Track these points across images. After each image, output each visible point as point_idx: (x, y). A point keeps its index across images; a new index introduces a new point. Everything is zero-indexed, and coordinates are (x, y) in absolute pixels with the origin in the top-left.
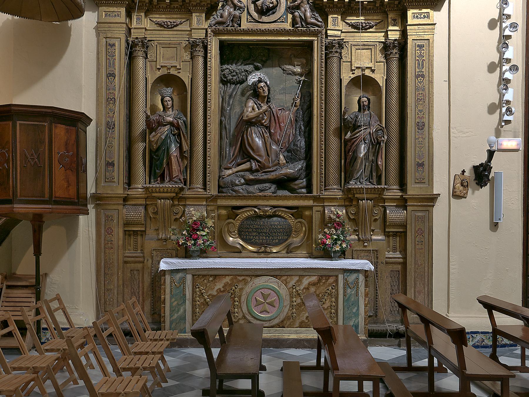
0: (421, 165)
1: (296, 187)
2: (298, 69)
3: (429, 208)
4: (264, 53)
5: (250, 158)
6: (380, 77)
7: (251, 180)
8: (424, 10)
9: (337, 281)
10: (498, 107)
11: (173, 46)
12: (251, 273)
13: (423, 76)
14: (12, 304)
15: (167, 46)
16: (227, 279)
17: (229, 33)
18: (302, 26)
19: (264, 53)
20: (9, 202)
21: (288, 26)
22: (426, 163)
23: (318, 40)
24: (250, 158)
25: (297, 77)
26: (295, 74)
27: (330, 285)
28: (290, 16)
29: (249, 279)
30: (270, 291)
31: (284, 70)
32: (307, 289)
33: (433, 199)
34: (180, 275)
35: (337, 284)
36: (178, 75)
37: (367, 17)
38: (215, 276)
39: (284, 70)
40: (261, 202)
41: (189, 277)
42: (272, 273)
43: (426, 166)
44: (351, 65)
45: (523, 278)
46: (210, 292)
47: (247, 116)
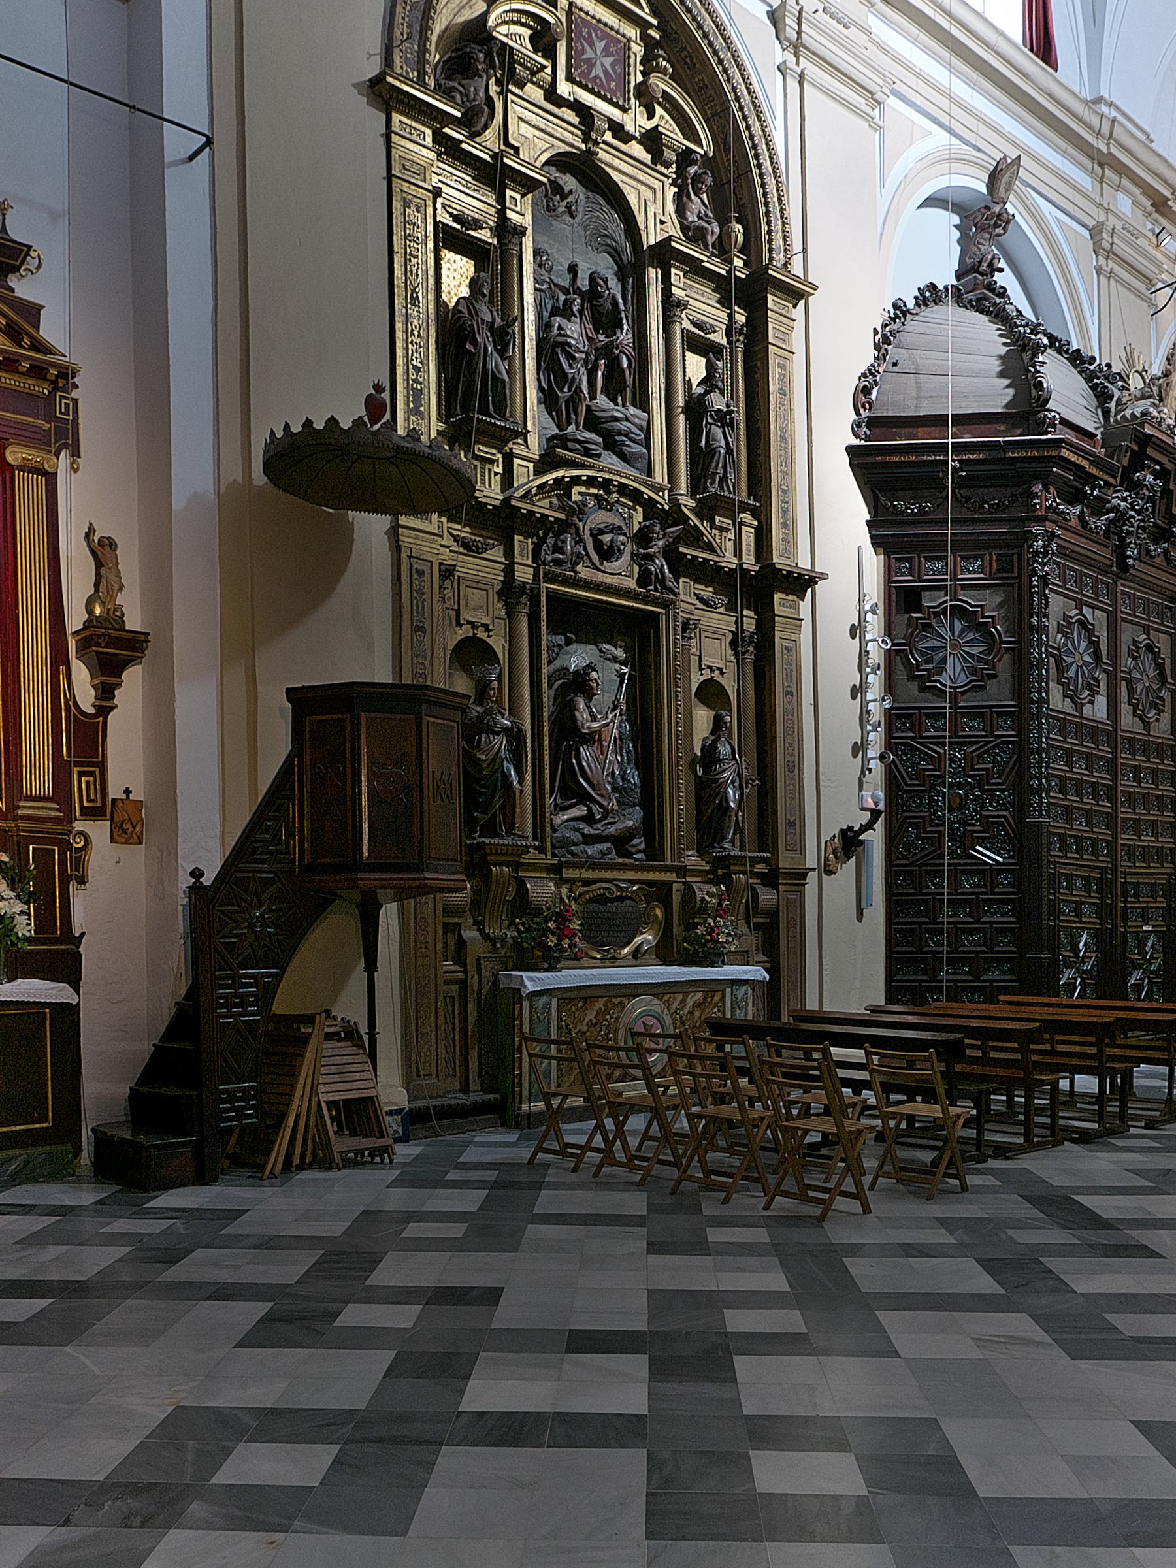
0: (792, 824)
1: (633, 850)
2: (620, 654)
3: (801, 888)
4: (578, 619)
5: (584, 798)
6: (729, 683)
7: (591, 836)
8: (791, 597)
9: (723, 999)
10: (859, 749)
11: (482, 586)
12: (624, 992)
13: (791, 693)
14: (334, 1069)
15: (474, 585)
16: (600, 1004)
17: (565, 581)
18: (656, 590)
19: (578, 619)
20: (418, 868)
21: (631, 584)
22: (797, 822)
23: (667, 614)
24: (584, 798)
25: (617, 666)
26: (615, 659)
27: (716, 1005)
28: (636, 569)
29: (625, 1000)
30: (655, 1021)
31: (601, 651)
32: (691, 1013)
33: (802, 875)
34: (544, 999)
35: (724, 1004)
36: (487, 640)
37: (475, 532)
38: (585, 999)
39: (601, 651)
40: (615, 875)
41: (554, 1001)
42: (655, 991)
43: (797, 825)
44: (700, 661)
45: (886, 985)
46: (579, 1028)
47: (588, 728)
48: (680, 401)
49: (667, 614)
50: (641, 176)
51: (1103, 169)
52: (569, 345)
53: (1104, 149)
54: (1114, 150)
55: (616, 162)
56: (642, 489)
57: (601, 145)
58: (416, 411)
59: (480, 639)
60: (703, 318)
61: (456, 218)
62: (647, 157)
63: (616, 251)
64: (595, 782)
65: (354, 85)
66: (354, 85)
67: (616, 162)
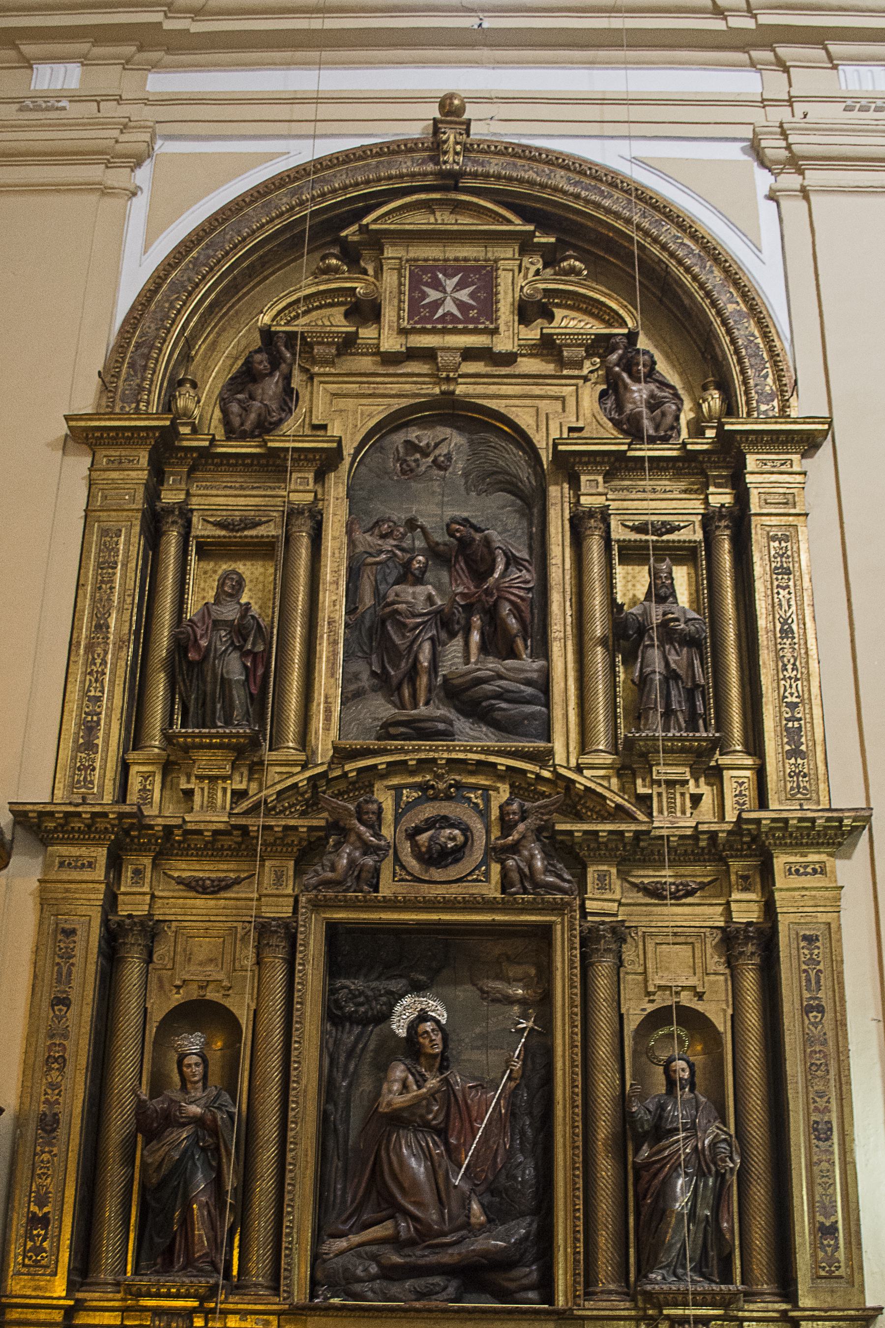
5: (395, 1210)
7: (395, 1267)
23: (562, 923)
24: (395, 1210)
31: (481, 990)
44: (646, 981)
48: (598, 627)
49: (562, 923)
50: (537, 390)
51: (773, 50)
52: (396, 612)
53: (750, 24)
54: (763, 19)
55: (493, 390)
56: (492, 759)
57: (460, 380)
58: (795, 753)
59: (210, 1002)
60: (646, 518)
61: (219, 525)
62: (549, 368)
63: (511, 483)
64: (406, 1185)
65: (48, 445)
66: (48, 445)
67: (493, 390)
